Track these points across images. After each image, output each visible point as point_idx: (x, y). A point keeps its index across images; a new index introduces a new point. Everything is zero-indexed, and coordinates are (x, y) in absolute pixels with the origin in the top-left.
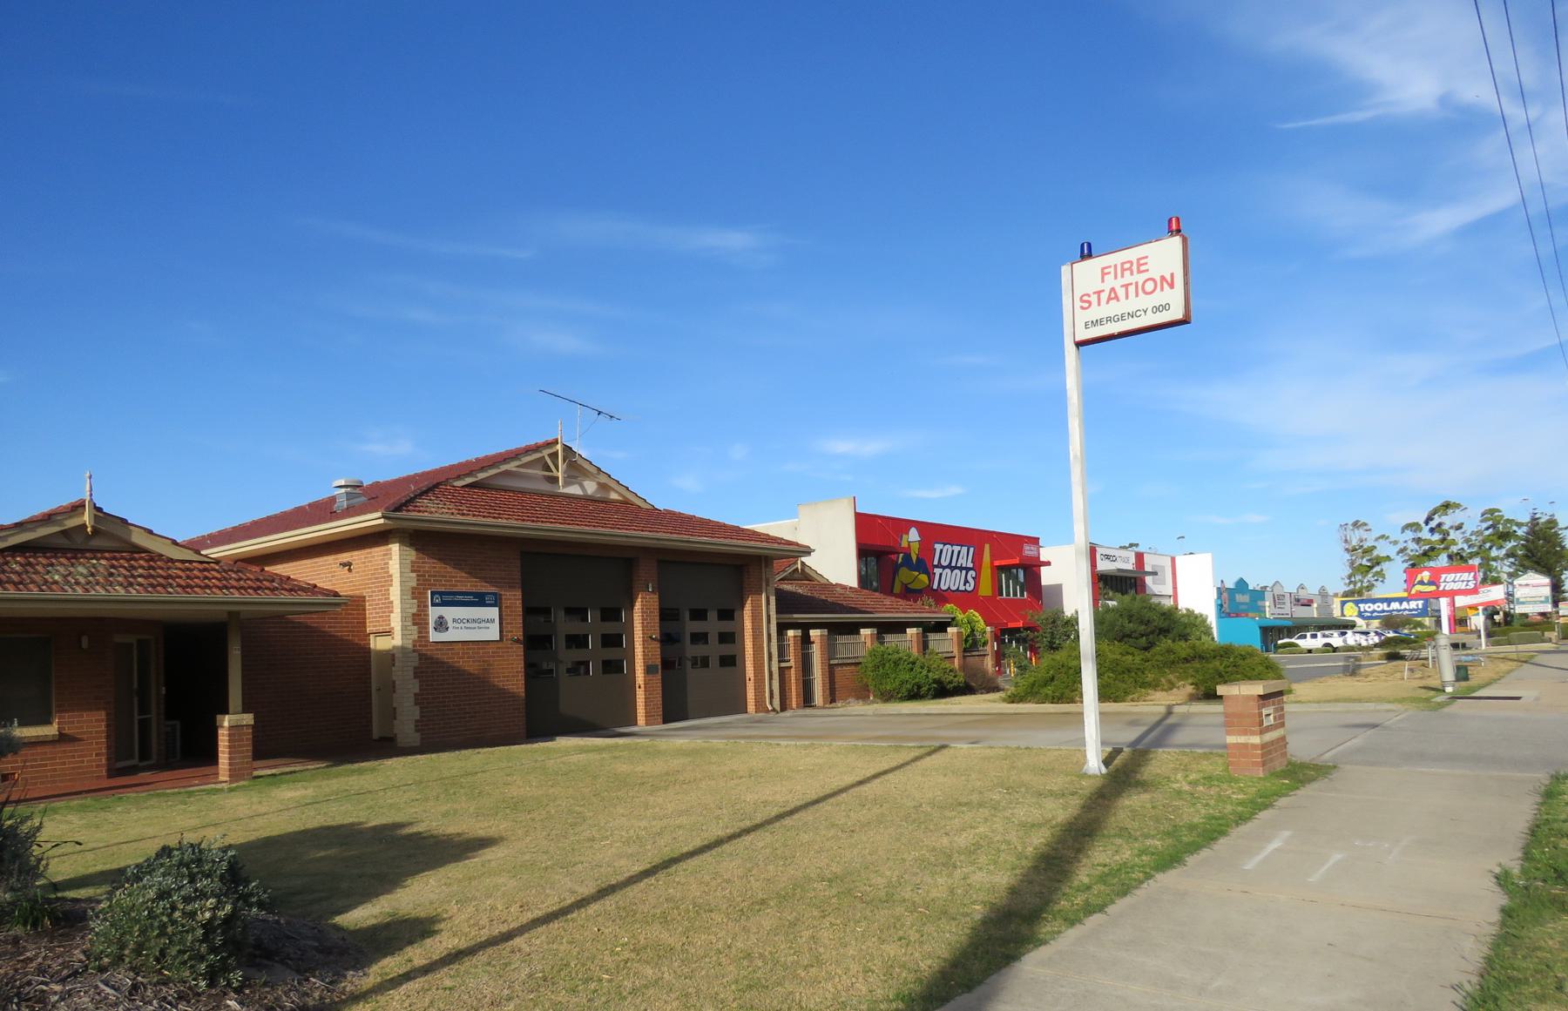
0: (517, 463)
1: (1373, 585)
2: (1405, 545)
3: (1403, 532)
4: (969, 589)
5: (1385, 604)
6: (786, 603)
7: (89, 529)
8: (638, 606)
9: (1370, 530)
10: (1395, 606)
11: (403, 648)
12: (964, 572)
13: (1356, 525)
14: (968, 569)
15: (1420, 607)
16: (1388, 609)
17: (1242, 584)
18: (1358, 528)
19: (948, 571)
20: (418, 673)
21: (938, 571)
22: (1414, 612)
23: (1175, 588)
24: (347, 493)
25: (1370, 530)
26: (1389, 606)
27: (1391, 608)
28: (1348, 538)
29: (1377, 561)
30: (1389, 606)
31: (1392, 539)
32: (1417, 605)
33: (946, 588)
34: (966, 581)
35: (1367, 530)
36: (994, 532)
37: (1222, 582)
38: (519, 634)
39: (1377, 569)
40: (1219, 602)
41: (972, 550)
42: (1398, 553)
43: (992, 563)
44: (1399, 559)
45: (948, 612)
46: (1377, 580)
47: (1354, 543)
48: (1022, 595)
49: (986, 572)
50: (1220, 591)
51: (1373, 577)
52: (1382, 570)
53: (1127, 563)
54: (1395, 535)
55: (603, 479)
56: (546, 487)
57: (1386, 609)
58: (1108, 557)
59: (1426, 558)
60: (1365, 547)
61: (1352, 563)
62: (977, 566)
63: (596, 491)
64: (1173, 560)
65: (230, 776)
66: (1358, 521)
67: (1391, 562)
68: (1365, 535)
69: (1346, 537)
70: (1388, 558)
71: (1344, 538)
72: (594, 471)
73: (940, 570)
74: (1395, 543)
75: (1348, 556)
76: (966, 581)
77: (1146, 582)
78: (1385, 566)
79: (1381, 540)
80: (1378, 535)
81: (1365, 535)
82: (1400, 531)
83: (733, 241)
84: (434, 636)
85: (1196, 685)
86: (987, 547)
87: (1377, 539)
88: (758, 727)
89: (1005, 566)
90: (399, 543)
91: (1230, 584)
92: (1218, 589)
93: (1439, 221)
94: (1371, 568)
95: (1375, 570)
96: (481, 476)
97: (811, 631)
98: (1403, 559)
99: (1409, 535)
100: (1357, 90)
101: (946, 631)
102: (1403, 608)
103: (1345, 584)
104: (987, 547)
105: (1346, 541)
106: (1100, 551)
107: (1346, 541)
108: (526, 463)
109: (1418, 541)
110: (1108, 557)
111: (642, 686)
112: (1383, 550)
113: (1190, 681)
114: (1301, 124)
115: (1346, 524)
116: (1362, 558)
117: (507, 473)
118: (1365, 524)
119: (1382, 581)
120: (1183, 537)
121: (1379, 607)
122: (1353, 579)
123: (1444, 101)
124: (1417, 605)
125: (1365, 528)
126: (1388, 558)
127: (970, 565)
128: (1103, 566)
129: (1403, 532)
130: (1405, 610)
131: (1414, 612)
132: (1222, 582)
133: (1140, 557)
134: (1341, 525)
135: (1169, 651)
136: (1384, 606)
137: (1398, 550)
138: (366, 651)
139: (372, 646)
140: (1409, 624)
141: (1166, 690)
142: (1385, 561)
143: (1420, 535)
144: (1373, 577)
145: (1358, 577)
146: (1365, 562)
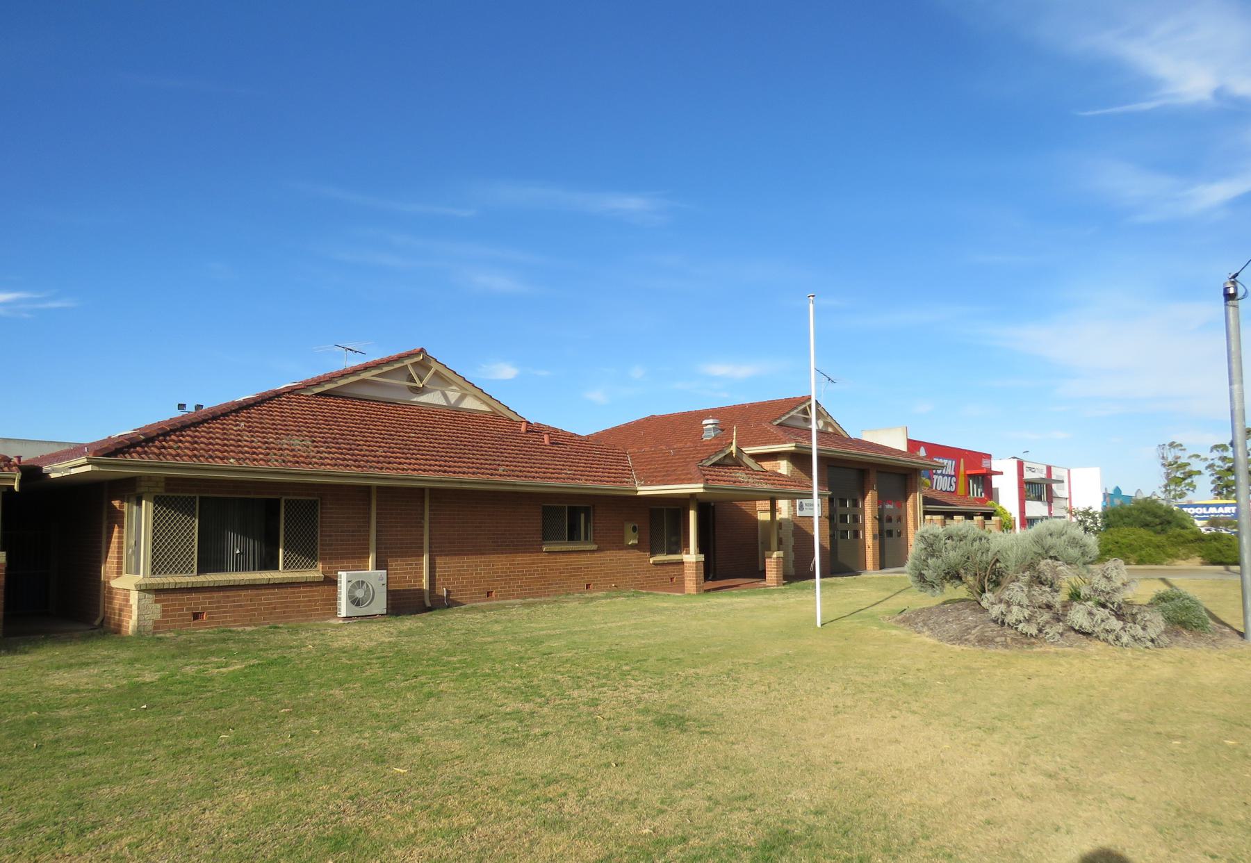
0: (796, 411)
1: (1185, 493)
2: (1212, 462)
3: (1212, 451)
4: (952, 490)
5: (1205, 509)
6: (927, 501)
7: (734, 455)
8: (868, 498)
9: (1184, 450)
10: (1212, 510)
11: (788, 519)
12: (950, 478)
13: (1172, 445)
14: (952, 476)
15: (1234, 511)
16: (1207, 513)
17: (1118, 490)
18: (1174, 447)
19: (941, 477)
20: (794, 534)
21: (935, 477)
22: (1228, 516)
23: (1070, 493)
24: (713, 428)
25: (1184, 450)
26: (1208, 510)
27: (1209, 512)
28: (1165, 455)
29: (1190, 475)
30: (1208, 510)
31: (1203, 457)
32: (1231, 510)
33: (939, 489)
34: (951, 485)
35: (1181, 450)
36: (966, 450)
37: (1106, 489)
38: (828, 515)
39: (1189, 481)
40: (1105, 504)
41: (954, 462)
42: (1207, 468)
43: (965, 472)
44: (1208, 472)
45: (990, 506)
46: (1188, 490)
47: (1170, 459)
48: (981, 495)
49: (962, 479)
50: (1106, 496)
51: (1185, 487)
52: (1192, 481)
53: (1040, 474)
54: (1205, 453)
55: (829, 420)
56: (803, 424)
57: (1205, 512)
58: (1030, 469)
59: (1229, 473)
60: (1179, 463)
61: (1168, 474)
62: (956, 475)
63: (823, 427)
64: (1069, 471)
65: (777, 583)
66: (1174, 442)
67: (1201, 476)
68: (1179, 454)
69: (1163, 454)
70: (1199, 473)
71: (1161, 456)
72: (826, 415)
73: (937, 476)
74: (1206, 459)
75: (1164, 470)
76: (951, 485)
77: (1053, 488)
78: (1195, 478)
79: (1193, 458)
80: (1192, 454)
81: (1179, 454)
82: (1209, 450)
83: (632, 204)
84: (799, 513)
85: (1202, 557)
86: (962, 460)
87: (1190, 457)
88: (833, 584)
89: (974, 474)
90: (788, 461)
91: (1111, 491)
92: (1104, 494)
93: (1216, 193)
94: (1184, 479)
95: (1186, 481)
96: (328, 387)
97: (769, 519)
98: (1210, 473)
99: (1216, 454)
100: (1147, 84)
101: (991, 519)
102: (1219, 512)
103: (1162, 492)
104: (962, 460)
105: (1163, 458)
106: (1026, 465)
107: (1163, 458)
108: (386, 372)
109: (1223, 459)
110: (1030, 469)
111: (871, 547)
112: (1196, 465)
113: (1197, 554)
114: (1098, 112)
115: (1164, 445)
116: (1177, 471)
117: (364, 381)
118: (1181, 445)
119: (1192, 491)
120: (1027, 452)
121: (1199, 511)
122: (1168, 488)
123: (1218, 93)
124: (1231, 510)
125: (1180, 448)
126: (1199, 473)
127: (953, 473)
128: (1028, 475)
129: (1212, 451)
130: (1221, 513)
131: (1228, 516)
132: (1106, 489)
133: (1049, 469)
134: (1159, 445)
135: (1180, 535)
136: (1204, 510)
137: (1206, 465)
138: (756, 520)
139: (759, 518)
140: (1231, 524)
141: (1184, 560)
142: (1196, 474)
143: (1225, 454)
144: (1185, 487)
145: (1172, 487)
146: (1178, 475)
